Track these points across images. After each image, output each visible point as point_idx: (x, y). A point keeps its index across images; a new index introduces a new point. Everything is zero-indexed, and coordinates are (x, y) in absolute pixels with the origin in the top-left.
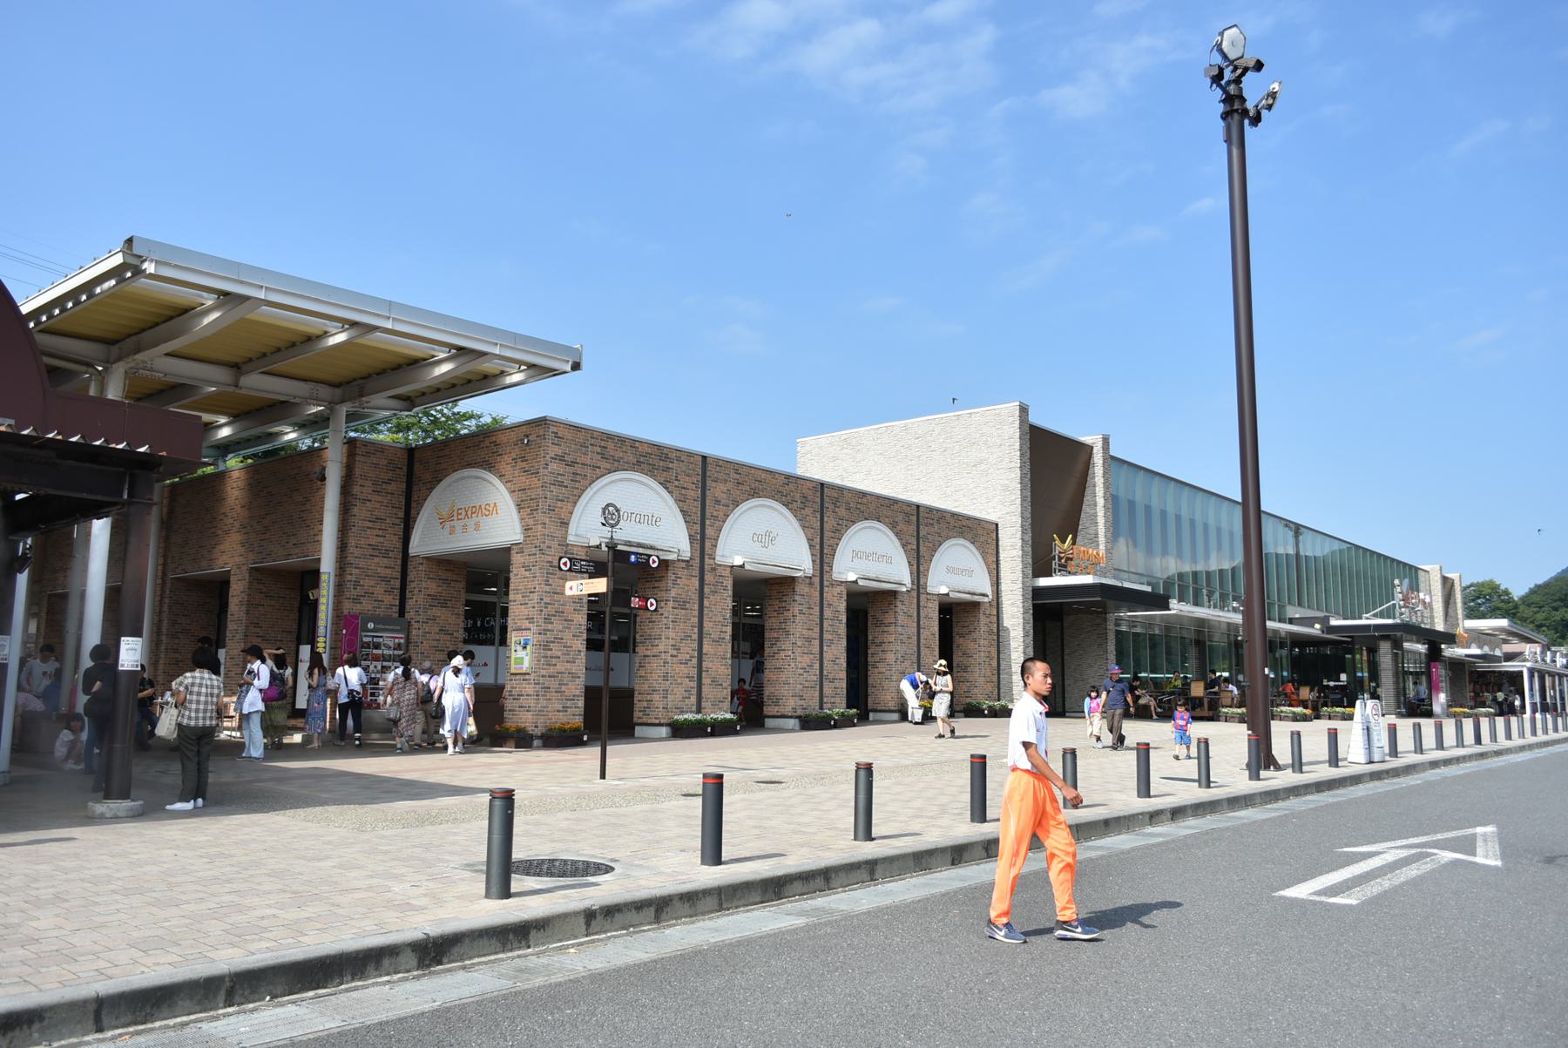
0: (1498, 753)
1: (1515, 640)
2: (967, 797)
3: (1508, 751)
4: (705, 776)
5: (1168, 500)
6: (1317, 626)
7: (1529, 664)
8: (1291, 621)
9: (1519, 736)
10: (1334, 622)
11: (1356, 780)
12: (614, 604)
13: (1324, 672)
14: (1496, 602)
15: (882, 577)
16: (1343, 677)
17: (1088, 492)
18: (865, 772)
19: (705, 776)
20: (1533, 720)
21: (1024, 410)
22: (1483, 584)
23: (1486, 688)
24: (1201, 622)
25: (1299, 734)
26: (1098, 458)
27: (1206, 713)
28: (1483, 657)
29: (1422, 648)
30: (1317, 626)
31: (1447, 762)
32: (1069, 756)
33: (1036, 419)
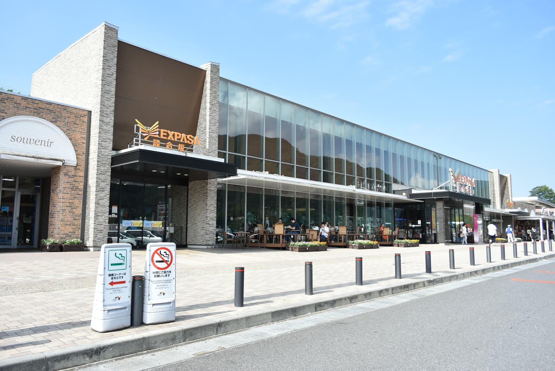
0: (520, 263)
1: (543, 207)
2: (354, 273)
3: (535, 260)
4: (236, 268)
5: (399, 150)
6: (404, 194)
7: (542, 217)
8: (394, 192)
9: (543, 250)
10: (414, 192)
11: (441, 281)
12: (15, 192)
13: (413, 220)
14: (547, 194)
15: (21, 154)
16: (419, 222)
17: (203, 101)
18: (240, 272)
19: (236, 268)
20: (543, 244)
21: (110, 31)
22: (542, 187)
23: (523, 227)
24: (352, 195)
25: (453, 250)
26: (208, 79)
27: (341, 244)
28: (518, 213)
29: (472, 207)
30: (404, 194)
31: (520, 263)
32: (451, 252)
33: (124, 37)
